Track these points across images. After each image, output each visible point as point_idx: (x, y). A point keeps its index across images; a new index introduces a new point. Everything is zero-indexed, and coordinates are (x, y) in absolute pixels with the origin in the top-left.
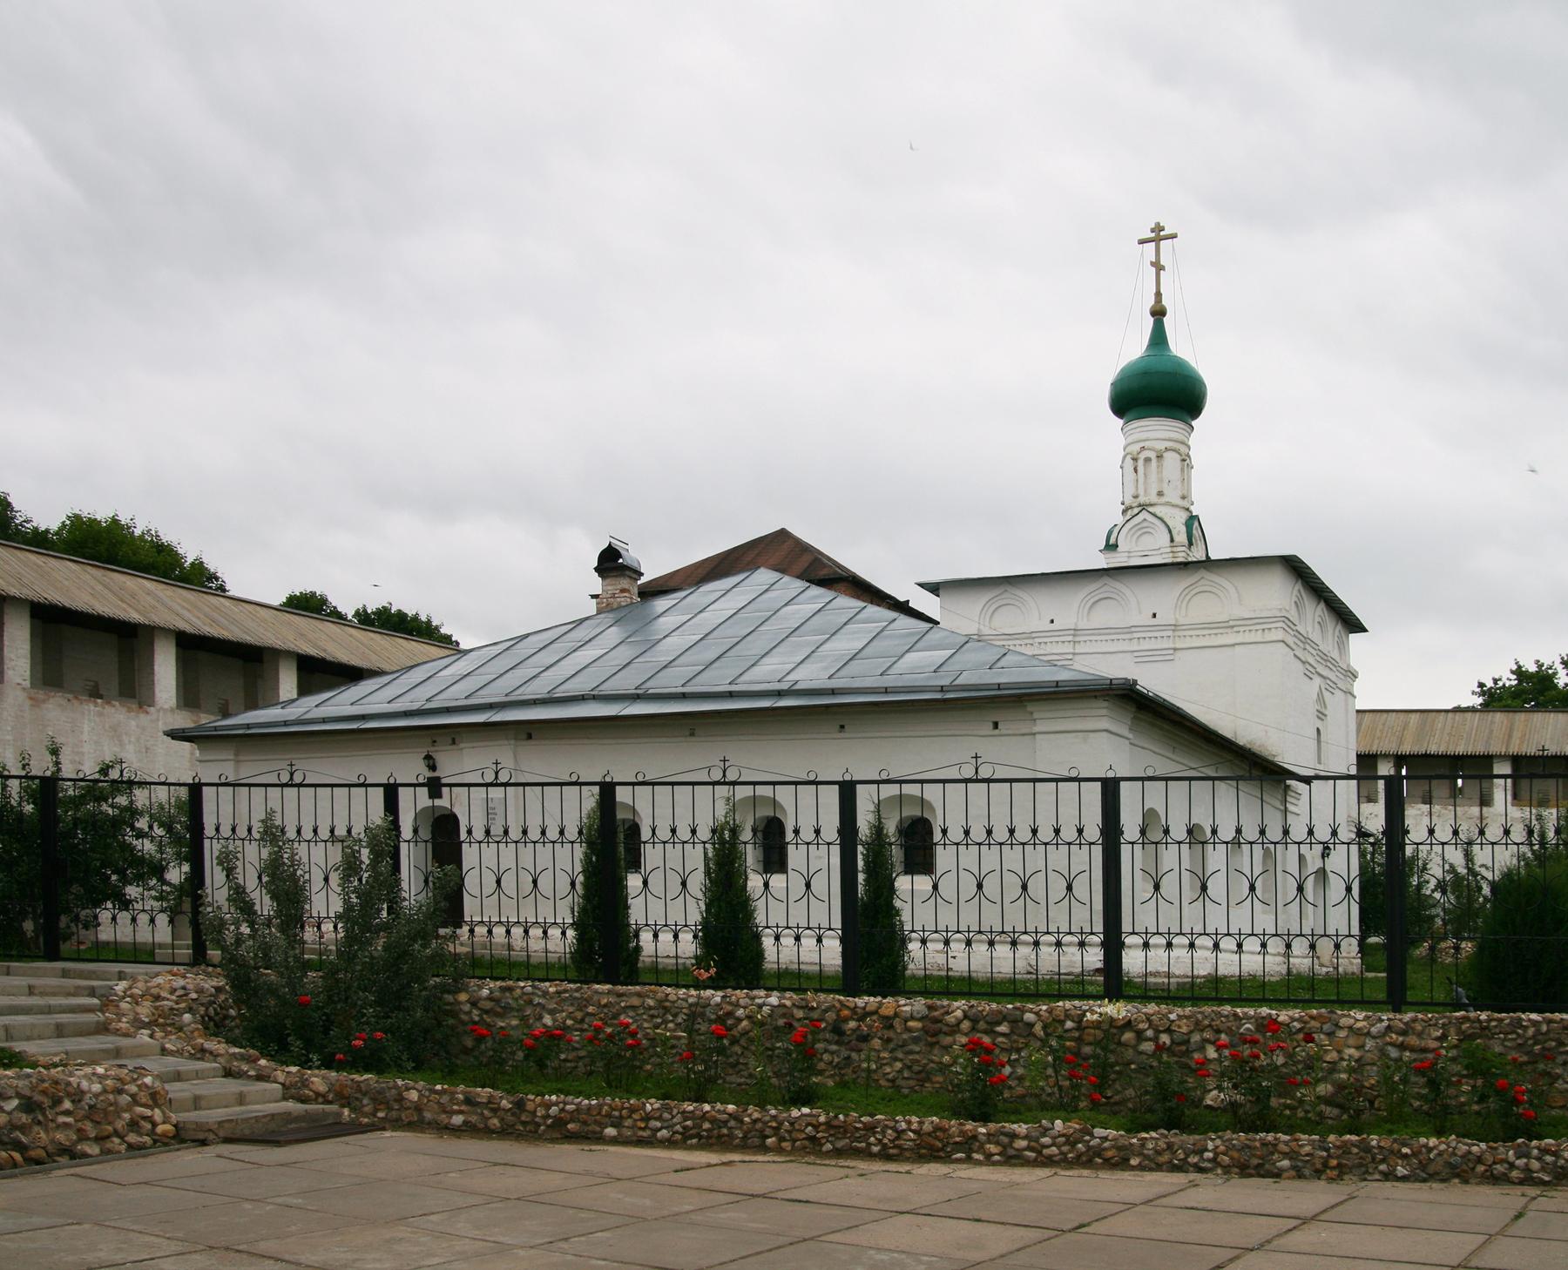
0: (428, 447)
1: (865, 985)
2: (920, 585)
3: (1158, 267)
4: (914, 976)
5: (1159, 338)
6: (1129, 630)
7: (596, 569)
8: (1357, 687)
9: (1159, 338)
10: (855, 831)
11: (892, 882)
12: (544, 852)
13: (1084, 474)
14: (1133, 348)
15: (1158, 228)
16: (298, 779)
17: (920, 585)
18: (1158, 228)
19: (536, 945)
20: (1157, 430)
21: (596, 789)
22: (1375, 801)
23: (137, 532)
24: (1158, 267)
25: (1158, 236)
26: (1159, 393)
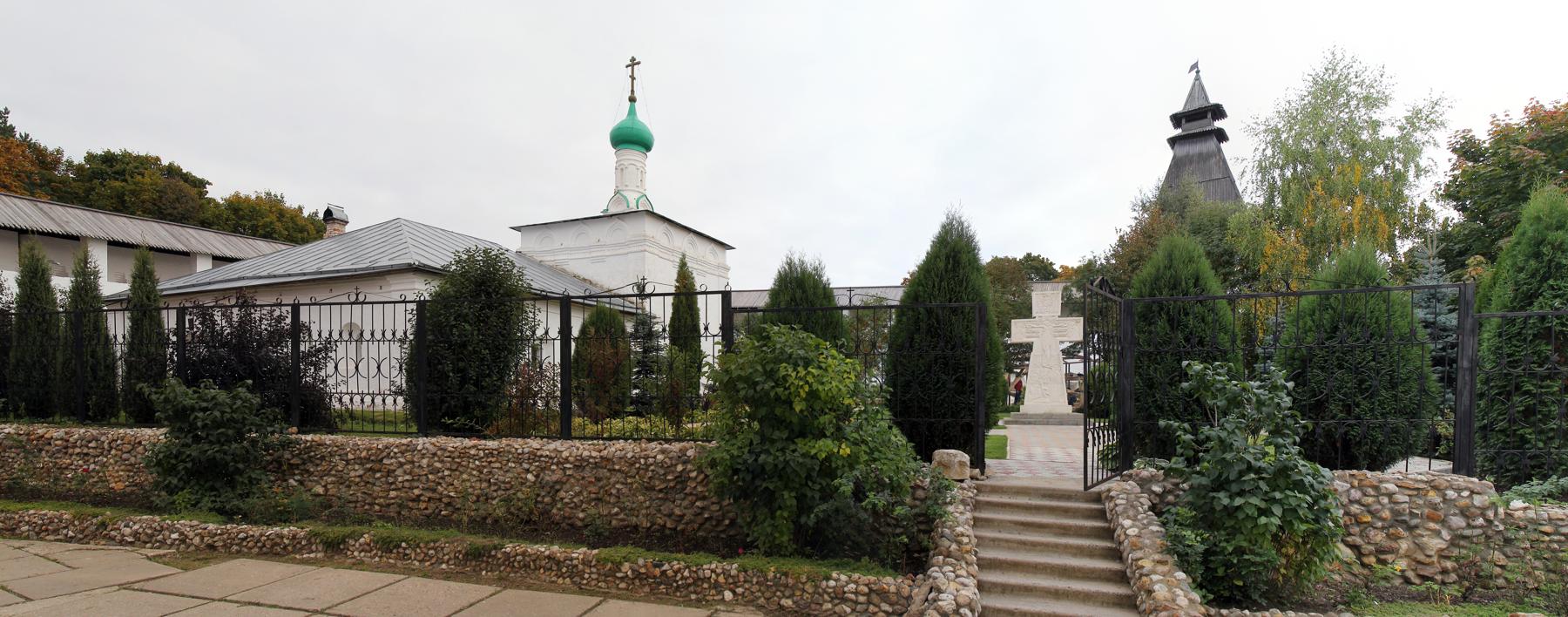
0: (22, 124)
1: (503, 423)
2: (683, 265)
3: (633, 78)
4: (211, 200)
5: (632, 112)
6: (590, 247)
7: (1029, 255)
8: (730, 274)
9: (632, 112)
10: (570, 328)
11: (48, 281)
12: (384, 347)
13: (591, 180)
14: (617, 115)
15: (633, 59)
16: (361, 298)
17: (683, 265)
18: (633, 59)
19: (357, 406)
20: (632, 155)
21: (414, 306)
22: (1005, 438)
23: (306, 214)
24: (633, 78)
25: (633, 63)
26: (630, 139)
